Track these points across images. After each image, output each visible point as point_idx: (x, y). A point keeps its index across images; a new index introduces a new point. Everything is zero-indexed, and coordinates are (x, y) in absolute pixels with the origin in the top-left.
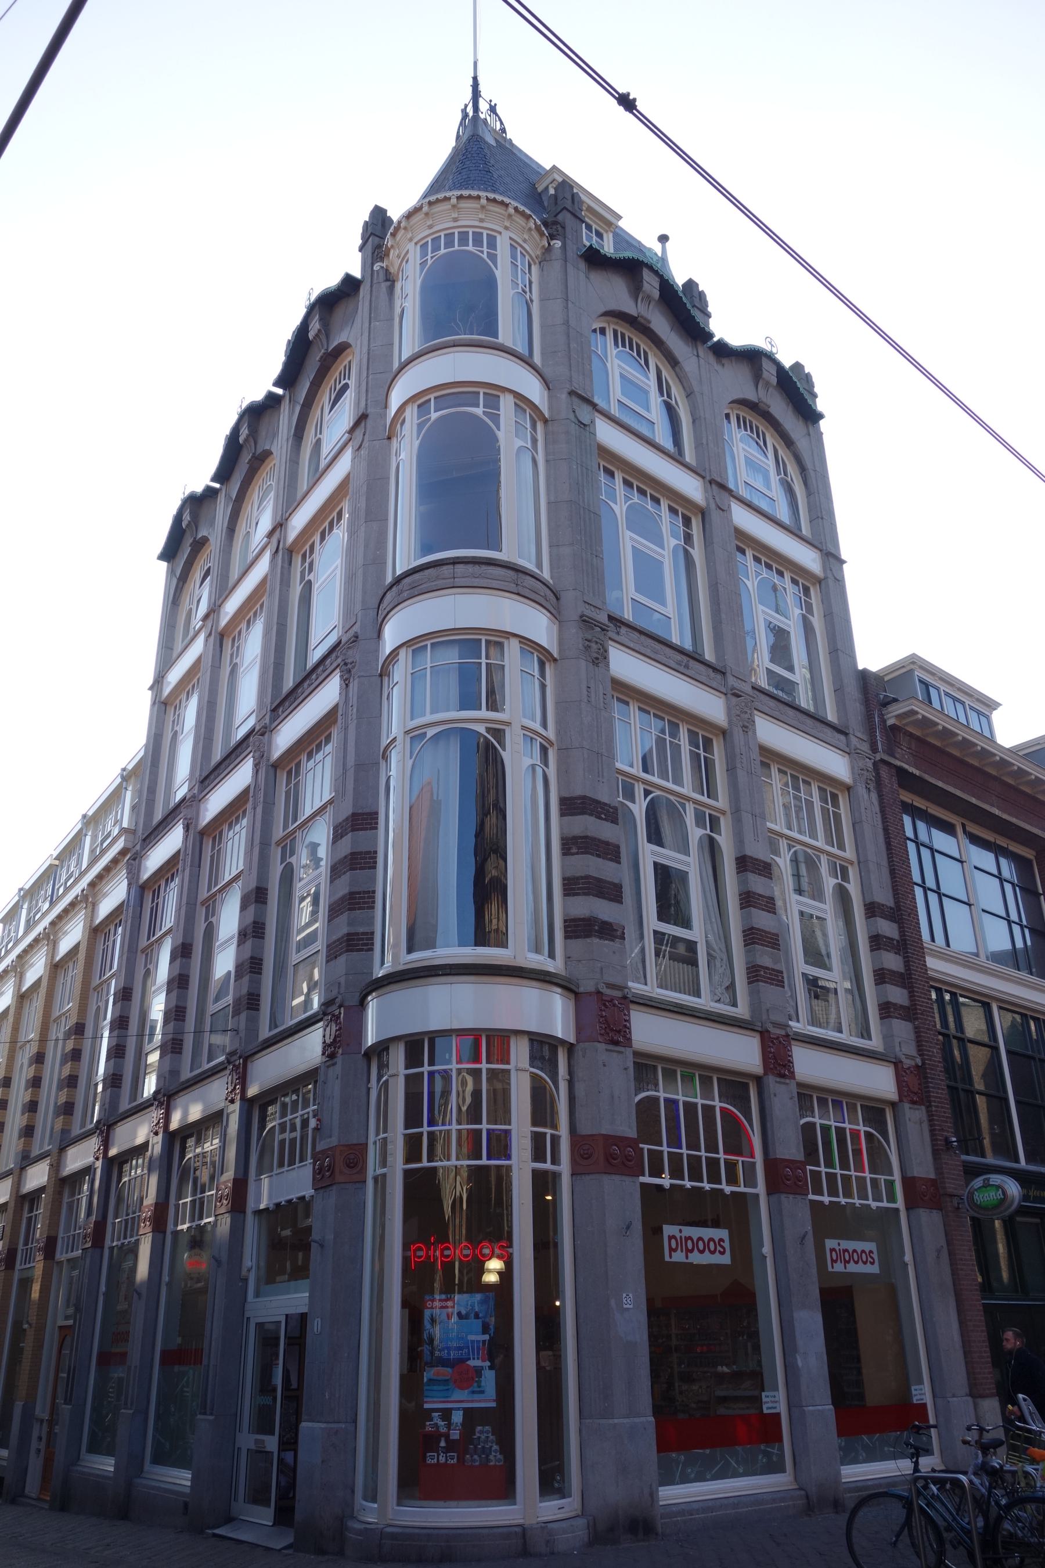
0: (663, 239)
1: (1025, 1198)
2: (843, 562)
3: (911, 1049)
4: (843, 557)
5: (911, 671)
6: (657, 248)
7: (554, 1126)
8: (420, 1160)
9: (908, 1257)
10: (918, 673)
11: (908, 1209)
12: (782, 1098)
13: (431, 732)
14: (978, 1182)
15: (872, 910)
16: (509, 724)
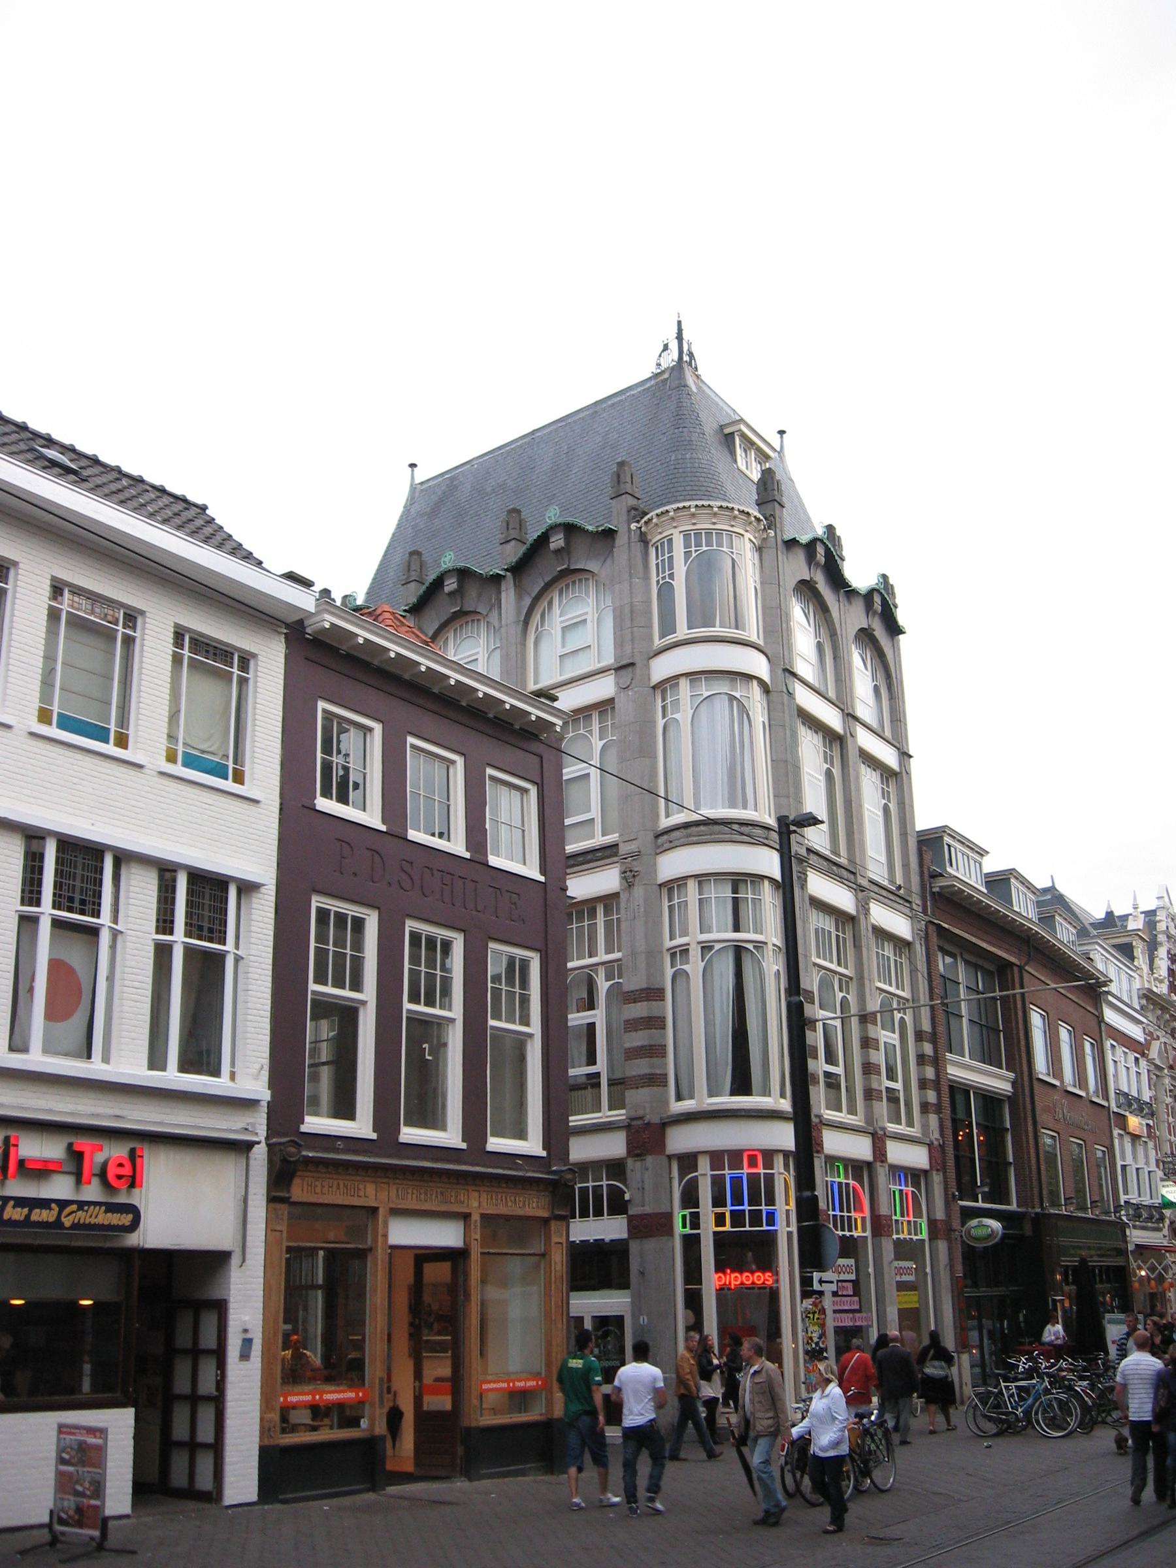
0: (782, 432)
1: (1004, 1228)
2: (911, 757)
3: (937, 1135)
4: (911, 753)
5: (942, 837)
6: (775, 441)
7: (862, 1211)
8: (724, 1225)
9: (871, 1270)
10: (947, 839)
11: (930, 1240)
12: (882, 1173)
13: (717, 946)
14: (974, 1222)
15: (919, 1036)
16: (766, 943)
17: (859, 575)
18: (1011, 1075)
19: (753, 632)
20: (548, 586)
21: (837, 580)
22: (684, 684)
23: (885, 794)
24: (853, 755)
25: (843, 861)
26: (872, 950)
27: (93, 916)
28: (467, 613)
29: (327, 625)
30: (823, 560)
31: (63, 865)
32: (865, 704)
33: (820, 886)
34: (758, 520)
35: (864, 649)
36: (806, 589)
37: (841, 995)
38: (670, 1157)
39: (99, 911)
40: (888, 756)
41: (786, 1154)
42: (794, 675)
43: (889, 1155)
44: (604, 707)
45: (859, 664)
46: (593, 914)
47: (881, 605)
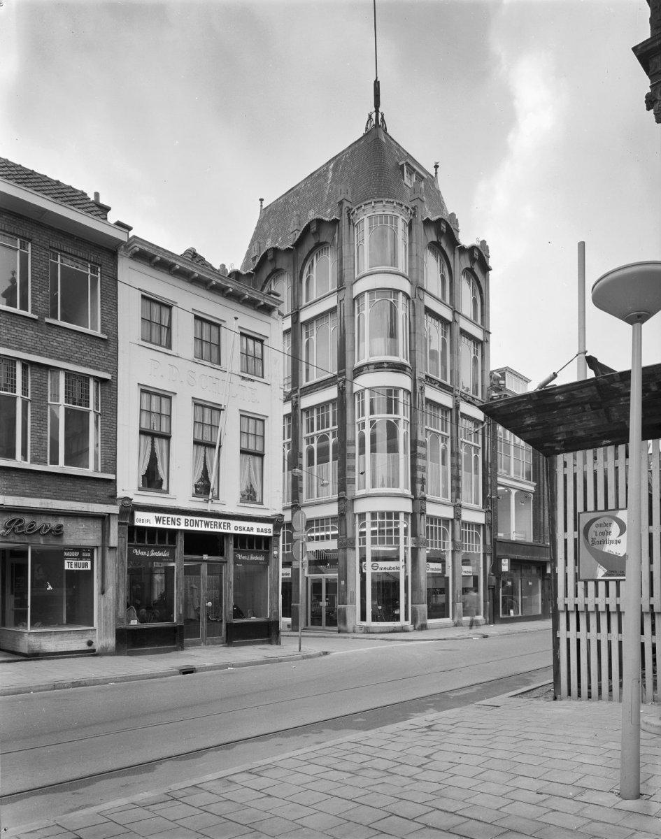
2: (490, 333)
6: (432, 172)
12: (457, 523)
17: (466, 240)
18: (535, 484)
19: (402, 267)
20: (311, 252)
21: (453, 242)
22: (366, 294)
23: (444, 334)
24: (457, 331)
25: (448, 383)
26: (464, 423)
27: (12, 392)
28: (278, 270)
29: (138, 249)
30: (477, 257)
31: (12, 368)
32: (466, 307)
33: (432, 393)
34: (408, 208)
35: (468, 280)
36: (435, 247)
37: (442, 444)
38: (355, 514)
39: (89, 405)
40: (478, 334)
41: (406, 514)
42: (424, 290)
43: (427, 510)
44: (333, 311)
45: (466, 290)
46: (328, 406)
47: (478, 260)
